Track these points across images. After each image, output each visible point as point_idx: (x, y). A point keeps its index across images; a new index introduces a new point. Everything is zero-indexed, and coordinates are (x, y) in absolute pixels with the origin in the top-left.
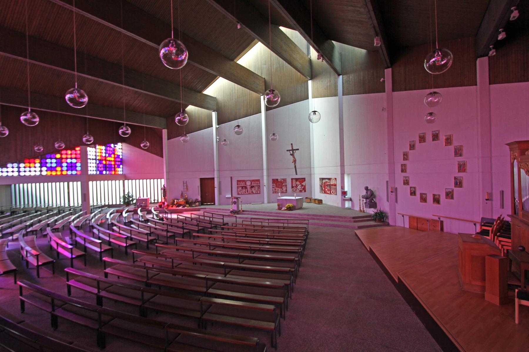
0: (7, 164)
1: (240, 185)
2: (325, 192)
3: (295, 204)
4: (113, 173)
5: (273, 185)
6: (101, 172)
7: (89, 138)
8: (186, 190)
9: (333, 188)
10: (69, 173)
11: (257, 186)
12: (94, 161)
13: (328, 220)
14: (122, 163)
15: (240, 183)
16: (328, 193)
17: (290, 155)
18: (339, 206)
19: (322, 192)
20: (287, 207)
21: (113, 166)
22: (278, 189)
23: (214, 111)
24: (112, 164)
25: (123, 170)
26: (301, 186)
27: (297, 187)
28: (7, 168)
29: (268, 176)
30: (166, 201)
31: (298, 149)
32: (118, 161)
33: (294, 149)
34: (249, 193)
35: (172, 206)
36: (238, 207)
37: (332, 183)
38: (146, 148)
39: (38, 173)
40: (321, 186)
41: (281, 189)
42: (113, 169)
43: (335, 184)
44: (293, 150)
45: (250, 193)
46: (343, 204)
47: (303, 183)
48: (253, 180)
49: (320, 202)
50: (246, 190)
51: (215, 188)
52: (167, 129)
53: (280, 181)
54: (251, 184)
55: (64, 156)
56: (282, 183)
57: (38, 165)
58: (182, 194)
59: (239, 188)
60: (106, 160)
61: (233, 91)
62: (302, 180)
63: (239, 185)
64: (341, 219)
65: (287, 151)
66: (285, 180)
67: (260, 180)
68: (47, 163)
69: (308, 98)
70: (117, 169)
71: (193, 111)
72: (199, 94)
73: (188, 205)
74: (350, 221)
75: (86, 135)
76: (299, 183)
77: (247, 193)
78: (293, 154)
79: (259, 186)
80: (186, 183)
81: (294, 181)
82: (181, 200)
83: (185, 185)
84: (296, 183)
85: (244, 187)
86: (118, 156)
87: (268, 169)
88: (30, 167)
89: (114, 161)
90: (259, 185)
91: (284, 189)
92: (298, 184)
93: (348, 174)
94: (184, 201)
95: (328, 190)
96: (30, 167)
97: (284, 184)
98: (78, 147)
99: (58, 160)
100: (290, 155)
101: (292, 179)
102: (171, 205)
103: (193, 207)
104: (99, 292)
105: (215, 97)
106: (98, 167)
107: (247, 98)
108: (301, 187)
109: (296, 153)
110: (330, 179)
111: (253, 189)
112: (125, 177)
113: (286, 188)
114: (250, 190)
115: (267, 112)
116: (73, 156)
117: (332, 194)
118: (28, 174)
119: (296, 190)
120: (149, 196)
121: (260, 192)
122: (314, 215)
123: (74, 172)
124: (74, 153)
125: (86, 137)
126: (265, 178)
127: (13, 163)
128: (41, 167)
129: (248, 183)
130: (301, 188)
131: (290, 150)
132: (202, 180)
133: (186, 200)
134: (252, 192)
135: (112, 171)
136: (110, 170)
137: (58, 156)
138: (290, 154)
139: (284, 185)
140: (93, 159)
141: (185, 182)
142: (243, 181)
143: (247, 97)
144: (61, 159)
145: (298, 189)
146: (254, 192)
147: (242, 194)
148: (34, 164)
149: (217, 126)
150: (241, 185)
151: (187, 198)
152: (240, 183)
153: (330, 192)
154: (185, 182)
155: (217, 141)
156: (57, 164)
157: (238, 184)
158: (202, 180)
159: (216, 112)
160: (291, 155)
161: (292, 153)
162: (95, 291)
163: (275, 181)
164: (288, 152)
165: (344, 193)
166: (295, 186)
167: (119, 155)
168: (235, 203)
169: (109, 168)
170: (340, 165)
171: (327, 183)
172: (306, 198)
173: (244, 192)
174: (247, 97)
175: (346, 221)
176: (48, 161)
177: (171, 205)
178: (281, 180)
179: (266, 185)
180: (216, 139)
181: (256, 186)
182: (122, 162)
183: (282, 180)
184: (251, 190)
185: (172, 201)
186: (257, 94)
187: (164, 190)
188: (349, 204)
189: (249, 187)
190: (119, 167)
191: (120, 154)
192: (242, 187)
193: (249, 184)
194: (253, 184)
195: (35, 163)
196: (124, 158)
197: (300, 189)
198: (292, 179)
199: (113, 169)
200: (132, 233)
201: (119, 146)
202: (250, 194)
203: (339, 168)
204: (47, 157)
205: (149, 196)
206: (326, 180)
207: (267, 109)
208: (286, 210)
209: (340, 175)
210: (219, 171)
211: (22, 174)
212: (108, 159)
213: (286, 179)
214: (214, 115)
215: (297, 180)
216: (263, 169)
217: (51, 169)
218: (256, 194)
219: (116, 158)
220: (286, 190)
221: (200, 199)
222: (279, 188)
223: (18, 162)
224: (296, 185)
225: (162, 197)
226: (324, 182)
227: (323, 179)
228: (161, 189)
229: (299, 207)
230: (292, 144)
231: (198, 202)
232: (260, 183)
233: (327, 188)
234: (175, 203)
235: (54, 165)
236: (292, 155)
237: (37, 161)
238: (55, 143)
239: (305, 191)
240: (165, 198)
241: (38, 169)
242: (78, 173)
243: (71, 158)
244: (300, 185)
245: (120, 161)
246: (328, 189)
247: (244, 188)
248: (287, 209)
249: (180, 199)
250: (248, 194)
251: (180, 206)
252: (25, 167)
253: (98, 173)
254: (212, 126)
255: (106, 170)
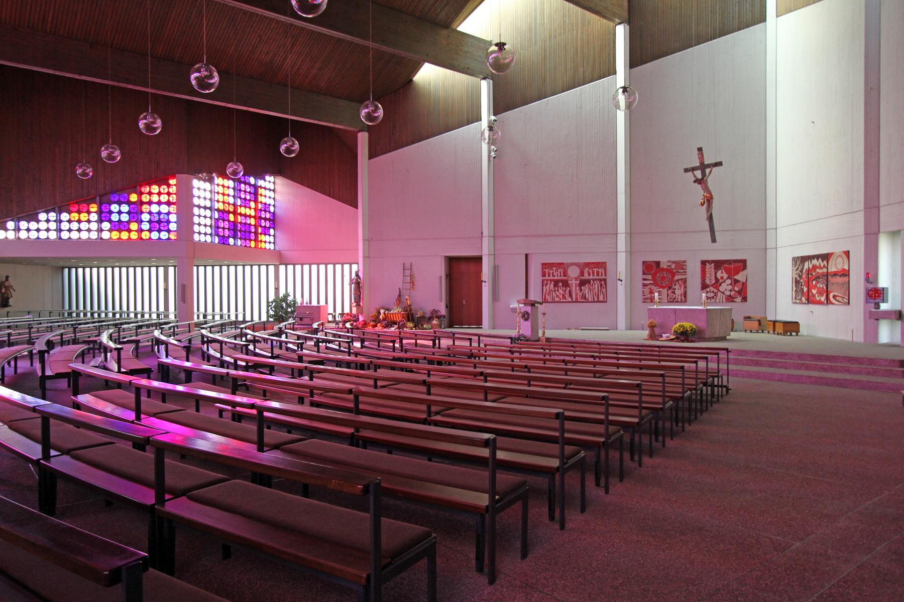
0: (37, 214)
1: (549, 276)
2: (810, 300)
3: (702, 324)
4: (253, 244)
5: (644, 279)
6: (224, 240)
7: (151, 120)
8: (408, 286)
9: (837, 283)
10: (155, 235)
11: (596, 280)
12: (208, 213)
13: (808, 368)
14: (274, 224)
15: (551, 272)
16: (820, 303)
17: (695, 182)
18: (855, 340)
19: (801, 299)
20: (676, 332)
21: (253, 230)
22: (661, 289)
23: (484, 78)
24: (250, 225)
25: (276, 239)
26: (731, 284)
27: (720, 285)
28: (38, 221)
29: (631, 253)
30: (362, 314)
31: (719, 164)
32: (265, 219)
33: (706, 163)
34: (574, 300)
35: (375, 326)
36: (534, 329)
37: (832, 269)
38: (293, 155)
39: (94, 235)
40: (797, 282)
41: (670, 291)
42: (253, 236)
43: (844, 270)
44: (703, 167)
45: (577, 298)
46: (872, 333)
47: (737, 273)
48: (587, 265)
49: (792, 327)
50: (567, 291)
51: (483, 283)
52: (368, 132)
53: (665, 267)
54: (582, 273)
55: (145, 198)
56: (673, 275)
57: (94, 217)
58: (400, 296)
59: (547, 284)
60: (235, 213)
61: (538, 21)
62: (738, 264)
63: (547, 278)
64: (854, 366)
65: (686, 170)
66: (681, 266)
67: (608, 266)
68: (111, 212)
69: (763, 19)
70: (262, 238)
71: (432, 80)
72: (444, 32)
73: (410, 324)
74: (890, 374)
75: (145, 114)
76: (725, 276)
77: (570, 300)
78: (703, 178)
79: (605, 280)
80: (411, 269)
81: (710, 268)
82: (396, 310)
83: (408, 272)
84: (716, 273)
85: (562, 281)
86: (266, 207)
87: (631, 234)
88: (79, 221)
89: (254, 217)
90: (604, 277)
91: (677, 292)
92: (722, 278)
93: (894, 234)
94: (403, 312)
95: (820, 293)
96: (79, 221)
97: (676, 278)
98: (173, 177)
99: (132, 206)
100: (695, 182)
101: (704, 263)
102: (372, 323)
103: (426, 329)
104: (46, 456)
105: (489, 40)
106: (218, 227)
107: (577, 37)
108: (730, 287)
109: (714, 177)
110: (826, 257)
111: (585, 289)
112: (280, 258)
113: (685, 287)
114: (578, 291)
115: (632, 70)
116: (164, 198)
117: (833, 304)
118: (75, 235)
119: (716, 294)
120: (322, 303)
121: (605, 296)
122: (758, 353)
123: (164, 235)
124: (166, 191)
125: (145, 118)
126: (622, 258)
127: (47, 212)
128: (100, 221)
129: (573, 272)
130: (730, 291)
131: (693, 169)
132: (451, 261)
133: (407, 311)
134: (584, 297)
135: (250, 240)
136: (246, 237)
137: (134, 198)
138: (694, 179)
139: (678, 281)
140: (205, 208)
141: (408, 266)
142: (560, 265)
143: (577, 33)
144: (138, 204)
145: (723, 293)
146: (589, 296)
147: (553, 302)
148: (86, 215)
149: (493, 118)
150: (551, 278)
151: (410, 305)
152: (551, 272)
153: (827, 298)
154: (408, 266)
155: (492, 159)
156: (132, 214)
157: (544, 275)
158: (451, 261)
159: (491, 82)
160: (697, 181)
161: (699, 176)
162: (34, 450)
163: (652, 269)
164: (690, 173)
165: (875, 294)
166: (714, 282)
167: (268, 203)
168: (526, 316)
169: (243, 233)
170: (862, 206)
171: (818, 270)
172: (748, 318)
173: (561, 297)
174: (577, 33)
175: (875, 373)
176: (115, 208)
177: (372, 323)
178: (669, 264)
179: (623, 277)
180: (489, 152)
181: (593, 280)
182: (274, 221)
183: (673, 266)
184: (581, 290)
185: (375, 313)
186: (605, 21)
187: (357, 284)
188: (892, 332)
189: (574, 283)
190: (266, 232)
191: (271, 202)
192: (556, 283)
193: (576, 276)
194: (586, 274)
195: (89, 213)
196: (278, 212)
197: (728, 293)
198: (704, 263)
199: (253, 236)
200: (224, 352)
201: (269, 182)
202: (577, 301)
203: (861, 217)
204: (112, 199)
205: (322, 303)
206: (815, 262)
207: (634, 61)
208: (672, 340)
209: (862, 239)
210: (494, 237)
211: (65, 235)
212: (242, 210)
213: (684, 262)
214: (485, 87)
215: (718, 264)
216: (617, 234)
217: (119, 226)
218: (594, 302)
219: (261, 210)
220: (685, 294)
221: (443, 311)
222: (664, 288)
223: (57, 209)
224: (717, 280)
225: (353, 301)
226: (806, 266)
227: (804, 259)
228: (351, 280)
229: (717, 335)
230: (700, 149)
231: (439, 317)
232: (605, 272)
233: (815, 287)
234: (381, 317)
235: (125, 218)
236: (700, 183)
237: (94, 208)
238: (101, 148)
239: (745, 299)
240: (358, 305)
241: (94, 226)
242: (173, 236)
243: (159, 203)
244: (729, 281)
245: (269, 220)
246: (819, 289)
247: (561, 284)
248: (677, 338)
249: (395, 307)
250: (572, 302)
251: (391, 326)
252: (70, 221)
253: (217, 240)
254: (479, 119)
255: (235, 237)
